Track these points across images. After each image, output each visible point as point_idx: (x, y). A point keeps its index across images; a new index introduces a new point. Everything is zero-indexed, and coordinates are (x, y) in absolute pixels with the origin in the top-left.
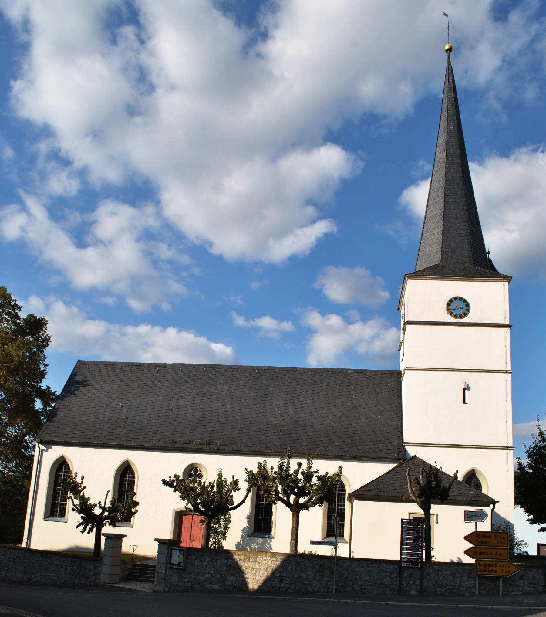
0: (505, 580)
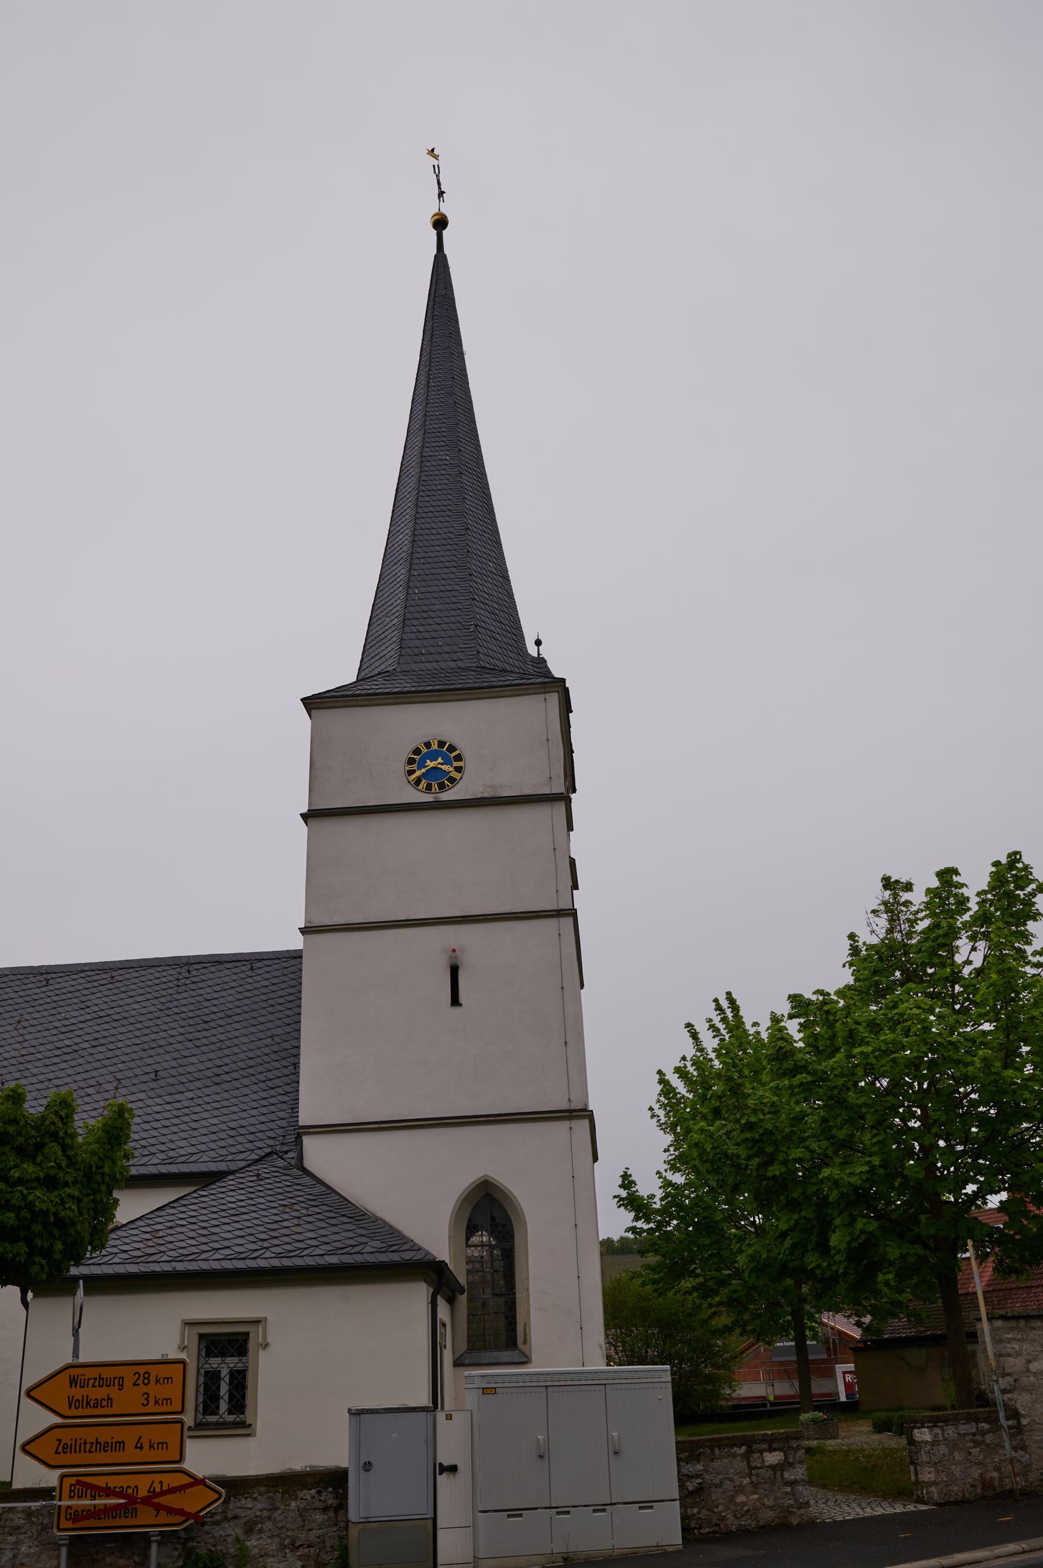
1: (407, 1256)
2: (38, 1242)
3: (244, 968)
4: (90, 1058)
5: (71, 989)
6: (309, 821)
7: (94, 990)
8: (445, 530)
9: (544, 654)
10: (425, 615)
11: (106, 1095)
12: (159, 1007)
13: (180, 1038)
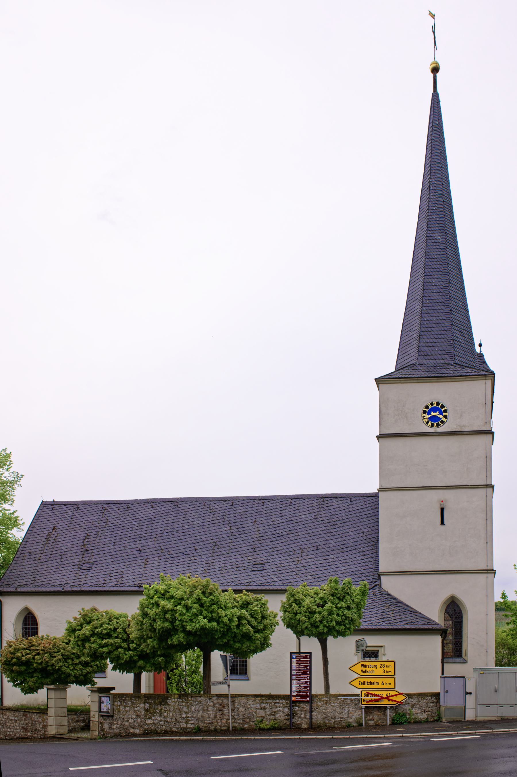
1: (435, 626)
2: (347, 626)
3: (347, 501)
4: (288, 539)
5: (274, 507)
6: (380, 439)
7: (284, 508)
8: (439, 283)
10: (429, 333)
11: (298, 555)
12: (314, 517)
13: (324, 532)
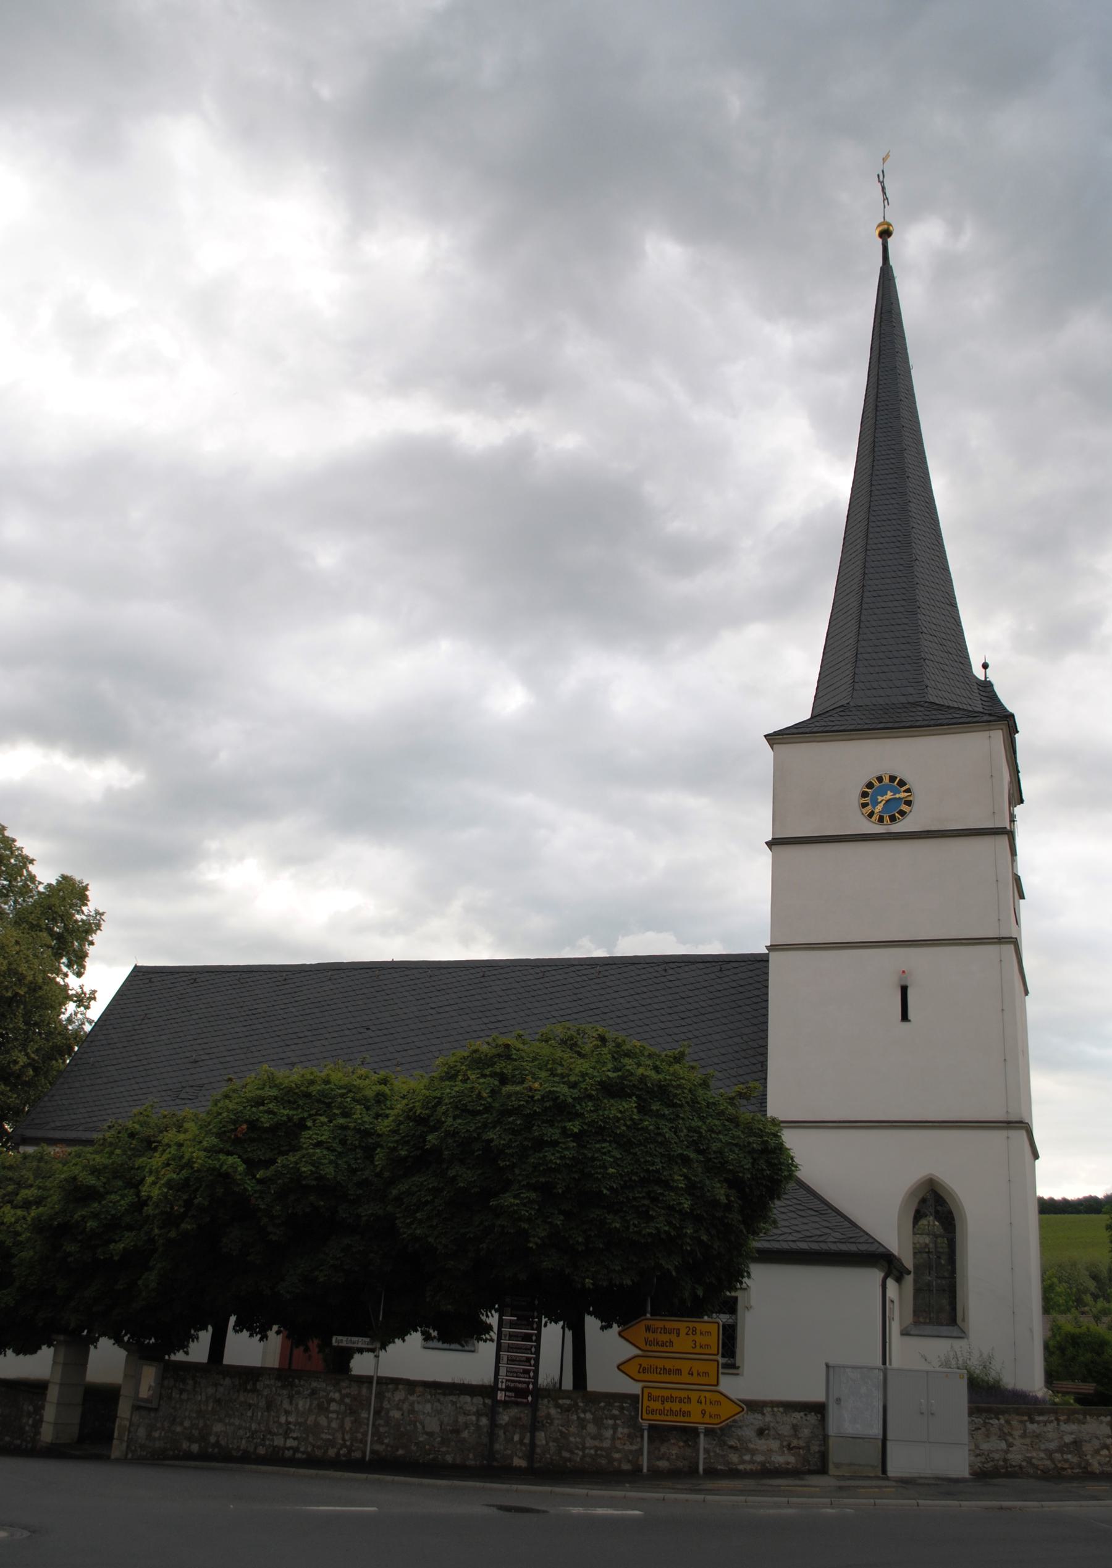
0: (709, 1432)
1: (863, 1248)
9: (991, 678)
